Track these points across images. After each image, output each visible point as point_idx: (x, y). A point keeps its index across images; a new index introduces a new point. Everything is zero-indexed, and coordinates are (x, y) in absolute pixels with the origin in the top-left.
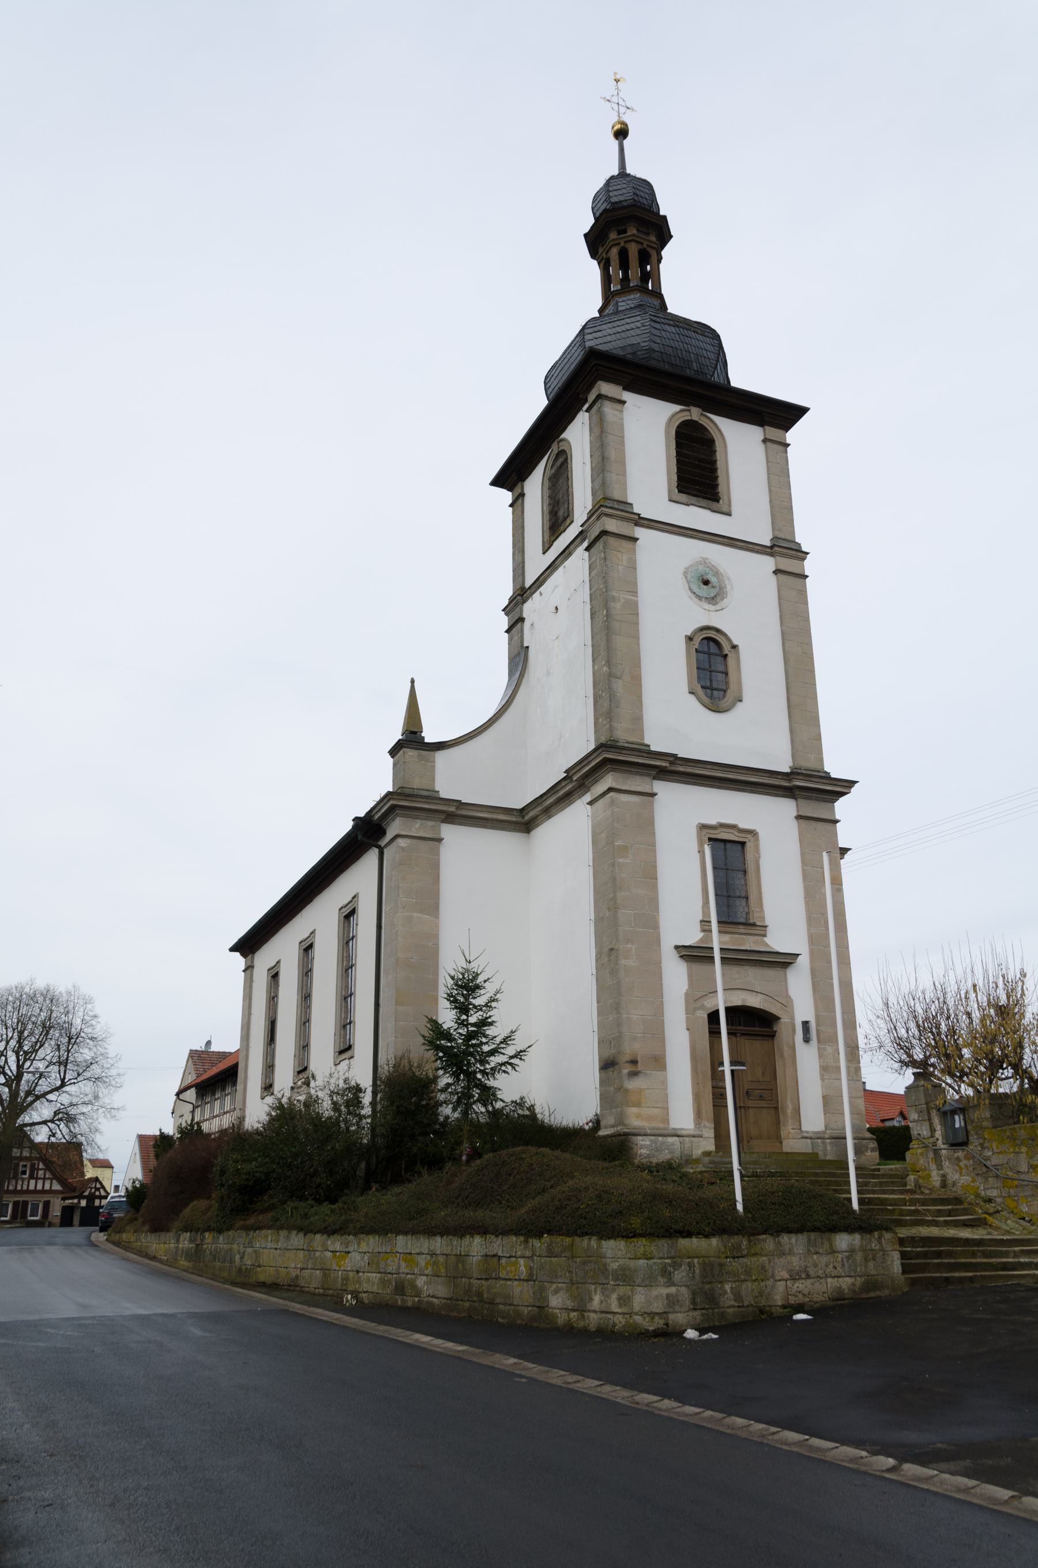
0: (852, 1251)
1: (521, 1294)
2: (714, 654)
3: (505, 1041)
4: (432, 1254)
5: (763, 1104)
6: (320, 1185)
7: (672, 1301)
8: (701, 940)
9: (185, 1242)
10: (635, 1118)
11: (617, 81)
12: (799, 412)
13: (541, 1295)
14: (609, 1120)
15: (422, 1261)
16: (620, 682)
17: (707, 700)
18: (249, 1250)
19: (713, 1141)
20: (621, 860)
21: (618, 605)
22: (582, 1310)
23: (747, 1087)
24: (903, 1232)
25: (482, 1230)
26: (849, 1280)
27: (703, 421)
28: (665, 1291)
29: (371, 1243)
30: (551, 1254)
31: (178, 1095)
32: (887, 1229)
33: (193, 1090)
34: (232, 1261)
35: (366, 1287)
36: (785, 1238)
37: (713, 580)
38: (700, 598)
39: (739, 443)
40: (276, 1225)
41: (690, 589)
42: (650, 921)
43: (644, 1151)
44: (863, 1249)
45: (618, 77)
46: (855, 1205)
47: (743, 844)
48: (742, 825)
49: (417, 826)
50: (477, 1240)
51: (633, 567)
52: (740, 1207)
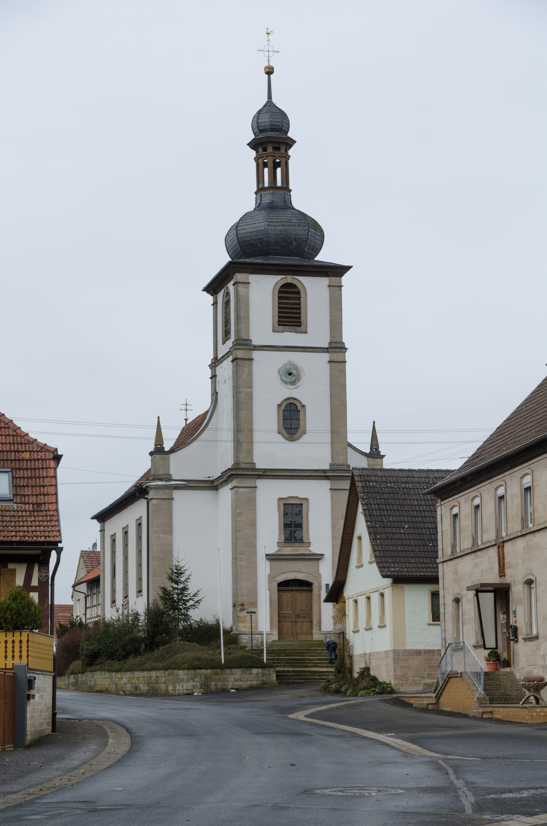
0: (258, 674)
1: (163, 686)
2: (293, 411)
3: (195, 595)
4: (144, 677)
5: (305, 620)
6: (119, 655)
7: (194, 686)
8: (278, 551)
9: (72, 679)
10: (244, 627)
11: (268, 34)
12: (347, 269)
13: (167, 687)
14: (234, 629)
15: (141, 679)
16: (242, 434)
17: (287, 435)
18: (93, 679)
19: (277, 636)
20: (239, 519)
21: (242, 395)
22: (174, 690)
23: (297, 613)
24: (278, 669)
25: (155, 669)
26: (256, 682)
27: (294, 282)
28: (192, 684)
29: (128, 674)
30: (169, 675)
31: (74, 587)
32: (272, 667)
33: (85, 584)
34: (87, 684)
35: (127, 689)
36: (234, 670)
37: (294, 372)
38: (286, 383)
39: (314, 288)
40: (102, 670)
41: (281, 379)
42: (252, 545)
43: (245, 641)
44: (262, 673)
45: (269, 32)
46: (265, 661)
47: (302, 504)
48: (301, 496)
49: (161, 493)
50: (154, 672)
51: (250, 374)
52: (223, 662)
